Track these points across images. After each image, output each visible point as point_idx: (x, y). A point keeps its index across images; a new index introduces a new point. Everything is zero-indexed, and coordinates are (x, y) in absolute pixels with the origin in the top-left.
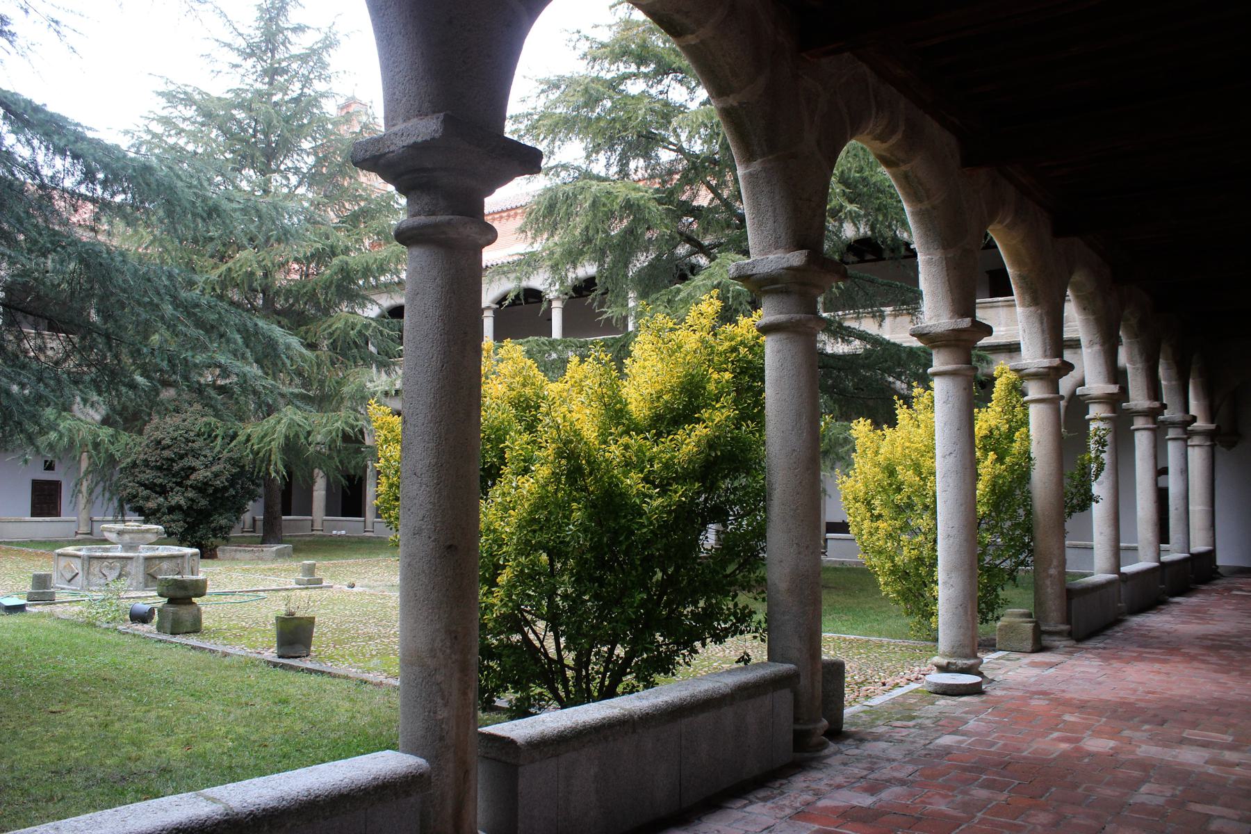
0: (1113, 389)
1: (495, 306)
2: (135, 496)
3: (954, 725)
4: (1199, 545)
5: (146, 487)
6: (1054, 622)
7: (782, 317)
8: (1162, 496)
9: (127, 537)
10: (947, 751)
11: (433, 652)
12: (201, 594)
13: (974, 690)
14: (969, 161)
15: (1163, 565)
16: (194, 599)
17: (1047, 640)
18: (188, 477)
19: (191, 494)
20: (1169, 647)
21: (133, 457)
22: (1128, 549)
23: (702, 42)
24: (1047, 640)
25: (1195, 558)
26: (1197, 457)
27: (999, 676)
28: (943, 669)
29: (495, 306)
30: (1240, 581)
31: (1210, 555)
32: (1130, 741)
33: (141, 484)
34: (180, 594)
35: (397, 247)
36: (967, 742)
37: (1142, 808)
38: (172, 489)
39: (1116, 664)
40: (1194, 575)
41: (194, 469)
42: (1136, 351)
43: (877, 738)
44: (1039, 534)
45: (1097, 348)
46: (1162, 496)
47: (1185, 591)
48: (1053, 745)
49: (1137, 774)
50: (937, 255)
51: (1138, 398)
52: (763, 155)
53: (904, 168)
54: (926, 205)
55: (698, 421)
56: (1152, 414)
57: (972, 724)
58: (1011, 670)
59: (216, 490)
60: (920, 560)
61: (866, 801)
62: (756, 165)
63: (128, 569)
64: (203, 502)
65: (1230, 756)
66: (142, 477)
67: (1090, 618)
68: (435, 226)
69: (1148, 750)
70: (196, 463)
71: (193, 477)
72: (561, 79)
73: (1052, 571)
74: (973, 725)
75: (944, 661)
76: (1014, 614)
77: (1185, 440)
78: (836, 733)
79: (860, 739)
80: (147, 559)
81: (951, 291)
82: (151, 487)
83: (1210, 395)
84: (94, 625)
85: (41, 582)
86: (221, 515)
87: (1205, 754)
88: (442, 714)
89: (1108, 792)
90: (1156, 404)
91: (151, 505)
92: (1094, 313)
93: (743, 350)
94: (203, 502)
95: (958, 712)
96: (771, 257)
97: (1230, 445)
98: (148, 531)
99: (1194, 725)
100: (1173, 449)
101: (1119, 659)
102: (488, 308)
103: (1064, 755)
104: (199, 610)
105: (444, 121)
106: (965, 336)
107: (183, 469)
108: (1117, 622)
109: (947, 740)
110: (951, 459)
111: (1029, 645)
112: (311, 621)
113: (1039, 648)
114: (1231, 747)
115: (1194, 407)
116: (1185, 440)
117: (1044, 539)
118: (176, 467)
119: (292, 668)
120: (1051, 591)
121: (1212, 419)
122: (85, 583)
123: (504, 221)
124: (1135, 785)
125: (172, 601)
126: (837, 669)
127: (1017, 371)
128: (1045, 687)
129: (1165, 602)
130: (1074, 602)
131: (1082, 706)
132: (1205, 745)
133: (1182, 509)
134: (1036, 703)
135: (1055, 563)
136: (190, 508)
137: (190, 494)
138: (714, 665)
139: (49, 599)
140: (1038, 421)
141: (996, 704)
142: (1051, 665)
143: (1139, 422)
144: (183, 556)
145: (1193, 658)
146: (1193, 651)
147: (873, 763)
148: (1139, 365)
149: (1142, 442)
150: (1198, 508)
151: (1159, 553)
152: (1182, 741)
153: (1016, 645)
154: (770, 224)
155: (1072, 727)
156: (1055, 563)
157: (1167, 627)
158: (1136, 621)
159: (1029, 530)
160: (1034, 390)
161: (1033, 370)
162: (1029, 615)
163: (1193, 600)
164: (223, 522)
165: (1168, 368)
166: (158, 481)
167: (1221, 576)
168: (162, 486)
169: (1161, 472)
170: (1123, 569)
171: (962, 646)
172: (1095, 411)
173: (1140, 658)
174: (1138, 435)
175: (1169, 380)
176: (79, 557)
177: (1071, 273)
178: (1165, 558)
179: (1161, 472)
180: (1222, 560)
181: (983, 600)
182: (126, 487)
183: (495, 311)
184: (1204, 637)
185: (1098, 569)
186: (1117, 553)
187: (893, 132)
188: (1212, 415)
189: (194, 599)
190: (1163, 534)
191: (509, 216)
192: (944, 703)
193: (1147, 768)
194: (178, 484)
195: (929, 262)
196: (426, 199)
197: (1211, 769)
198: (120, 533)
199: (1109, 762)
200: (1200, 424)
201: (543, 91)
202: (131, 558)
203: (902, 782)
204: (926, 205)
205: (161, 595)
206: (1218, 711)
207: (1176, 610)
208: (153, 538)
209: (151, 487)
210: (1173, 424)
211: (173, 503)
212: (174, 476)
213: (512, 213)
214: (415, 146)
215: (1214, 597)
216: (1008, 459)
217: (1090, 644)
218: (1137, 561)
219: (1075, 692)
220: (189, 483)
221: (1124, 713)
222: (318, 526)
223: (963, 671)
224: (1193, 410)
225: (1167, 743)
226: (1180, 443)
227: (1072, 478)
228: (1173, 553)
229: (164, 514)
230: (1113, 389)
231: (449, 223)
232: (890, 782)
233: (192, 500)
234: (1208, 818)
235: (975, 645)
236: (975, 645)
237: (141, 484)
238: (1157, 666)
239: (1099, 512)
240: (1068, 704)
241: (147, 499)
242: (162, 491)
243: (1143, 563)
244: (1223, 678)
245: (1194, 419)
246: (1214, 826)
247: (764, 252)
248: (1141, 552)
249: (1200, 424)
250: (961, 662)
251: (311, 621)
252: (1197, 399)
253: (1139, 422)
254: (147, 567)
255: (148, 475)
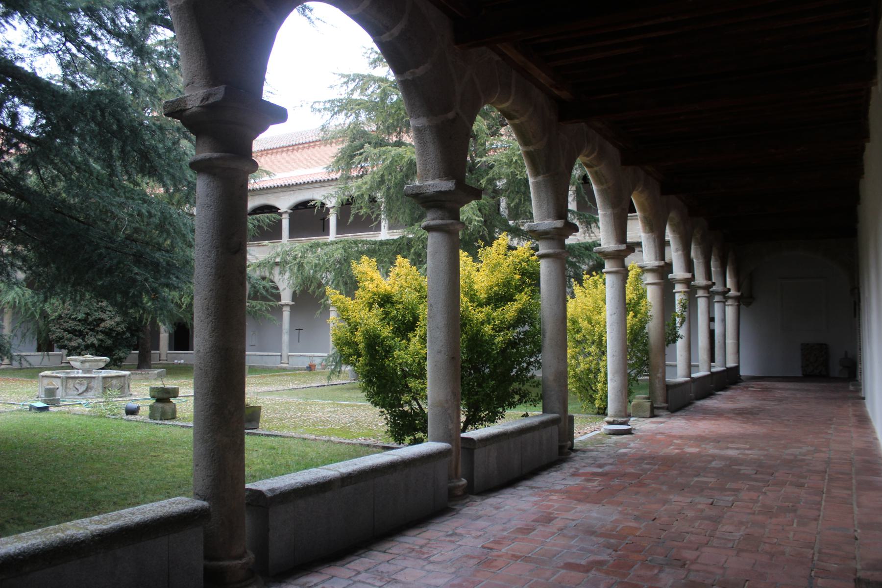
0: (689, 275)
1: (290, 211)
2: (61, 338)
3: (625, 446)
4: (731, 364)
5: (69, 332)
6: (660, 403)
7: (550, 251)
8: (712, 333)
9: (87, 365)
10: (625, 454)
11: (447, 401)
12: (176, 396)
13: (628, 432)
14: (625, 162)
15: (712, 373)
16: (172, 400)
17: (656, 412)
18: (98, 325)
19: (101, 337)
20: (718, 414)
21: (59, 312)
22: (695, 366)
23: (522, 123)
24: (656, 412)
25: (729, 370)
26: (730, 311)
27: (637, 427)
28: (609, 423)
29: (290, 211)
30: (752, 384)
31: (736, 369)
32: (705, 448)
33: (65, 330)
34: (165, 396)
35: (424, 231)
36: (633, 451)
37: (714, 468)
38: (87, 333)
39: (693, 421)
40: (728, 379)
41: (102, 320)
42: (699, 253)
43: (592, 451)
44: (652, 356)
45: (680, 252)
46: (712, 333)
47: (724, 388)
48: (672, 450)
49: (710, 458)
50: (609, 212)
51: (700, 280)
52: (544, 174)
53: (596, 169)
54: (604, 187)
55: (516, 300)
56: (707, 288)
57: (632, 445)
58: (643, 425)
59: (118, 334)
60: (589, 370)
61: (600, 470)
62: (540, 178)
63: (92, 384)
64: (109, 342)
65: (747, 452)
66: (66, 325)
67: (678, 400)
68: (446, 225)
69: (712, 451)
70: (104, 316)
71: (102, 325)
72: (358, 75)
73: (659, 375)
74: (631, 446)
75: (611, 419)
76: (640, 398)
77: (724, 302)
78: (572, 449)
79: (584, 451)
80: (104, 378)
81: (616, 229)
82: (73, 332)
83: (737, 275)
84: (104, 417)
85: (51, 392)
86: (120, 350)
87: (738, 452)
88: (451, 426)
89: (700, 464)
90: (709, 283)
91: (74, 344)
92: (679, 233)
93: (524, 264)
94: (109, 342)
95: (624, 441)
96: (546, 222)
97: (748, 304)
98: (100, 360)
99: (732, 442)
100: (717, 307)
101: (694, 419)
102: (286, 212)
103: (678, 454)
104: (175, 405)
105: (456, 184)
106: (622, 254)
107: (95, 320)
108: (690, 403)
109: (623, 451)
110: (615, 317)
111: (648, 413)
112: (260, 408)
113: (653, 416)
114: (748, 449)
115: (729, 283)
116: (724, 302)
117: (654, 358)
118: (90, 319)
119: (254, 434)
120: (658, 385)
121: (738, 289)
122: (64, 394)
123: (289, 153)
124: (710, 462)
125: (159, 400)
126: (571, 419)
127: (641, 267)
128: (661, 431)
129: (713, 394)
130: (670, 392)
131: (681, 437)
132: (738, 449)
133: (722, 342)
134: (658, 437)
135: (660, 370)
136: (100, 346)
137: (101, 337)
138: (511, 419)
139: (56, 403)
140: (652, 295)
141: (640, 437)
142: (662, 423)
143: (700, 293)
144: (124, 376)
145: (730, 418)
146: (730, 415)
147: (595, 459)
148: (701, 261)
149: (702, 304)
150: (730, 341)
151: (710, 367)
152: (728, 448)
153: (641, 414)
154: (545, 206)
155: (678, 445)
156: (660, 370)
157: (716, 405)
158: (699, 403)
159: (647, 353)
160: (649, 278)
161: (649, 267)
162: (648, 398)
163: (728, 393)
164: (122, 355)
165: (716, 260)
166: (78, 328)
167: (742, 381)
168: (81, 332)
169: (712, 319)
170: (693, 376)
171: (620, 411)
172: (679, 288)
173: (704, 419)
174: (699, 300)
175: (716, 268)
176: (59, 377)
177: (669, 213)
178: (713, 370)
179: (712, 319)
180: (743, 372)
181: (628, 388)
182: (54, 332)
183: (290, 215)
184: (735, 409)
185: (679, 376)
186: (690, 367)
187: (593, 153)
188: (738, 287)
189: (172, 400)
190: (712, 359)
191: (293, 149)
192: (615, 438)
193: (714, 457)
194: (91, 330)
195: (605, 215)
196: (440, 213)
197: (740, 456)
198: (83, 362)
199: (698, 456)
200: (733, 293)
201: (345, 83)
202: (94, 378)
203: (611, 464)
204: (604, 187)
205: (153, 397)
206: (742, 437)
207: (719, 398)
208: (102, 365)
209: (73, 332)
210: (718, 293)
211: (89, 342)
212: (88, 324)
213: (296, 147)
214: (440, 192)
215: (739, 391)
216: (639, 316)
217: (678, 413)
218: (698, 371)
219: (675, 432)
220: (99, 329)
221: (701, 439)
222: (163, 357)
223: (621, 424)
224: (728, 286)
225: (721, 449)
226: (721, 304)
227: (668, 325)
228: (717, 368)
229: (82, 350)
230: (689, 275)
231: (452, 224)
232: (605, 464)
233: (101, 340)
234: (740, 470)
235: (625, 415)
236: (625, 415)
237: (65, 330)
238: (713, 422)
239: (680, 344)
240: (675, 437)
241: (70, 340)
242: (81, 334)
243: (701, 372)
244: (745, 426)
245: (729, 290)
246: (742, 472)
247: (542, 219)
248: (700, 367)
249: (733, 293)
250: (620, 420)
251: (260, 408)
252: (731, 278)
253: (700, 293)
254: (104, 383)
255: (71, 324)
